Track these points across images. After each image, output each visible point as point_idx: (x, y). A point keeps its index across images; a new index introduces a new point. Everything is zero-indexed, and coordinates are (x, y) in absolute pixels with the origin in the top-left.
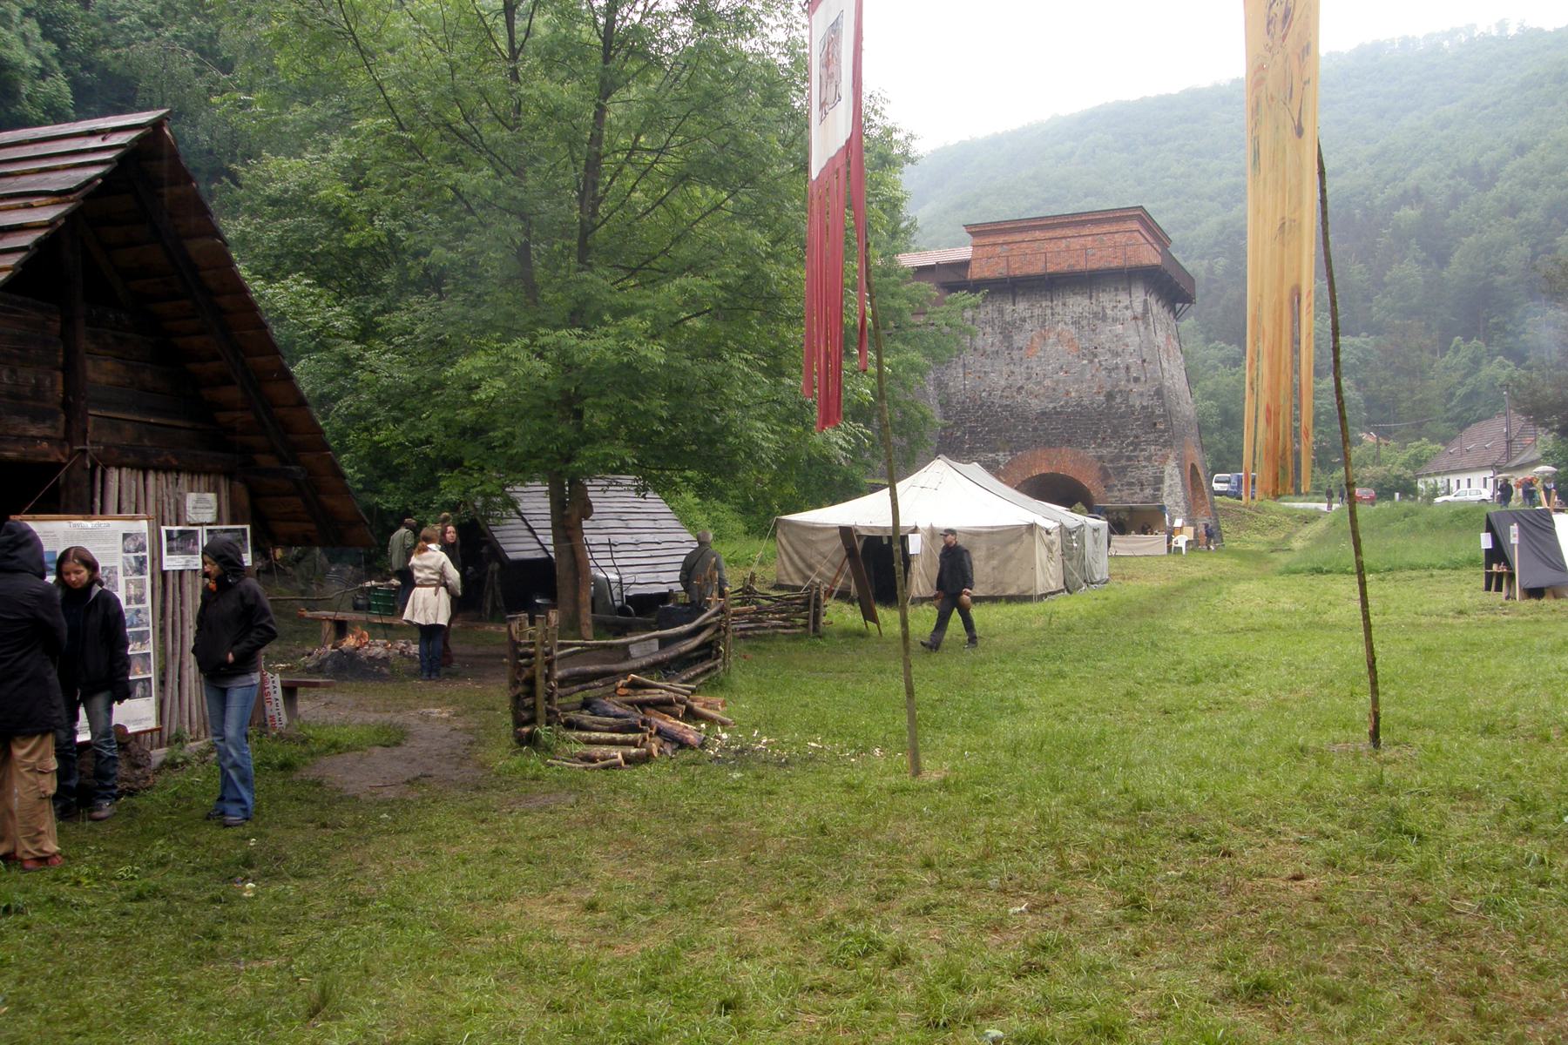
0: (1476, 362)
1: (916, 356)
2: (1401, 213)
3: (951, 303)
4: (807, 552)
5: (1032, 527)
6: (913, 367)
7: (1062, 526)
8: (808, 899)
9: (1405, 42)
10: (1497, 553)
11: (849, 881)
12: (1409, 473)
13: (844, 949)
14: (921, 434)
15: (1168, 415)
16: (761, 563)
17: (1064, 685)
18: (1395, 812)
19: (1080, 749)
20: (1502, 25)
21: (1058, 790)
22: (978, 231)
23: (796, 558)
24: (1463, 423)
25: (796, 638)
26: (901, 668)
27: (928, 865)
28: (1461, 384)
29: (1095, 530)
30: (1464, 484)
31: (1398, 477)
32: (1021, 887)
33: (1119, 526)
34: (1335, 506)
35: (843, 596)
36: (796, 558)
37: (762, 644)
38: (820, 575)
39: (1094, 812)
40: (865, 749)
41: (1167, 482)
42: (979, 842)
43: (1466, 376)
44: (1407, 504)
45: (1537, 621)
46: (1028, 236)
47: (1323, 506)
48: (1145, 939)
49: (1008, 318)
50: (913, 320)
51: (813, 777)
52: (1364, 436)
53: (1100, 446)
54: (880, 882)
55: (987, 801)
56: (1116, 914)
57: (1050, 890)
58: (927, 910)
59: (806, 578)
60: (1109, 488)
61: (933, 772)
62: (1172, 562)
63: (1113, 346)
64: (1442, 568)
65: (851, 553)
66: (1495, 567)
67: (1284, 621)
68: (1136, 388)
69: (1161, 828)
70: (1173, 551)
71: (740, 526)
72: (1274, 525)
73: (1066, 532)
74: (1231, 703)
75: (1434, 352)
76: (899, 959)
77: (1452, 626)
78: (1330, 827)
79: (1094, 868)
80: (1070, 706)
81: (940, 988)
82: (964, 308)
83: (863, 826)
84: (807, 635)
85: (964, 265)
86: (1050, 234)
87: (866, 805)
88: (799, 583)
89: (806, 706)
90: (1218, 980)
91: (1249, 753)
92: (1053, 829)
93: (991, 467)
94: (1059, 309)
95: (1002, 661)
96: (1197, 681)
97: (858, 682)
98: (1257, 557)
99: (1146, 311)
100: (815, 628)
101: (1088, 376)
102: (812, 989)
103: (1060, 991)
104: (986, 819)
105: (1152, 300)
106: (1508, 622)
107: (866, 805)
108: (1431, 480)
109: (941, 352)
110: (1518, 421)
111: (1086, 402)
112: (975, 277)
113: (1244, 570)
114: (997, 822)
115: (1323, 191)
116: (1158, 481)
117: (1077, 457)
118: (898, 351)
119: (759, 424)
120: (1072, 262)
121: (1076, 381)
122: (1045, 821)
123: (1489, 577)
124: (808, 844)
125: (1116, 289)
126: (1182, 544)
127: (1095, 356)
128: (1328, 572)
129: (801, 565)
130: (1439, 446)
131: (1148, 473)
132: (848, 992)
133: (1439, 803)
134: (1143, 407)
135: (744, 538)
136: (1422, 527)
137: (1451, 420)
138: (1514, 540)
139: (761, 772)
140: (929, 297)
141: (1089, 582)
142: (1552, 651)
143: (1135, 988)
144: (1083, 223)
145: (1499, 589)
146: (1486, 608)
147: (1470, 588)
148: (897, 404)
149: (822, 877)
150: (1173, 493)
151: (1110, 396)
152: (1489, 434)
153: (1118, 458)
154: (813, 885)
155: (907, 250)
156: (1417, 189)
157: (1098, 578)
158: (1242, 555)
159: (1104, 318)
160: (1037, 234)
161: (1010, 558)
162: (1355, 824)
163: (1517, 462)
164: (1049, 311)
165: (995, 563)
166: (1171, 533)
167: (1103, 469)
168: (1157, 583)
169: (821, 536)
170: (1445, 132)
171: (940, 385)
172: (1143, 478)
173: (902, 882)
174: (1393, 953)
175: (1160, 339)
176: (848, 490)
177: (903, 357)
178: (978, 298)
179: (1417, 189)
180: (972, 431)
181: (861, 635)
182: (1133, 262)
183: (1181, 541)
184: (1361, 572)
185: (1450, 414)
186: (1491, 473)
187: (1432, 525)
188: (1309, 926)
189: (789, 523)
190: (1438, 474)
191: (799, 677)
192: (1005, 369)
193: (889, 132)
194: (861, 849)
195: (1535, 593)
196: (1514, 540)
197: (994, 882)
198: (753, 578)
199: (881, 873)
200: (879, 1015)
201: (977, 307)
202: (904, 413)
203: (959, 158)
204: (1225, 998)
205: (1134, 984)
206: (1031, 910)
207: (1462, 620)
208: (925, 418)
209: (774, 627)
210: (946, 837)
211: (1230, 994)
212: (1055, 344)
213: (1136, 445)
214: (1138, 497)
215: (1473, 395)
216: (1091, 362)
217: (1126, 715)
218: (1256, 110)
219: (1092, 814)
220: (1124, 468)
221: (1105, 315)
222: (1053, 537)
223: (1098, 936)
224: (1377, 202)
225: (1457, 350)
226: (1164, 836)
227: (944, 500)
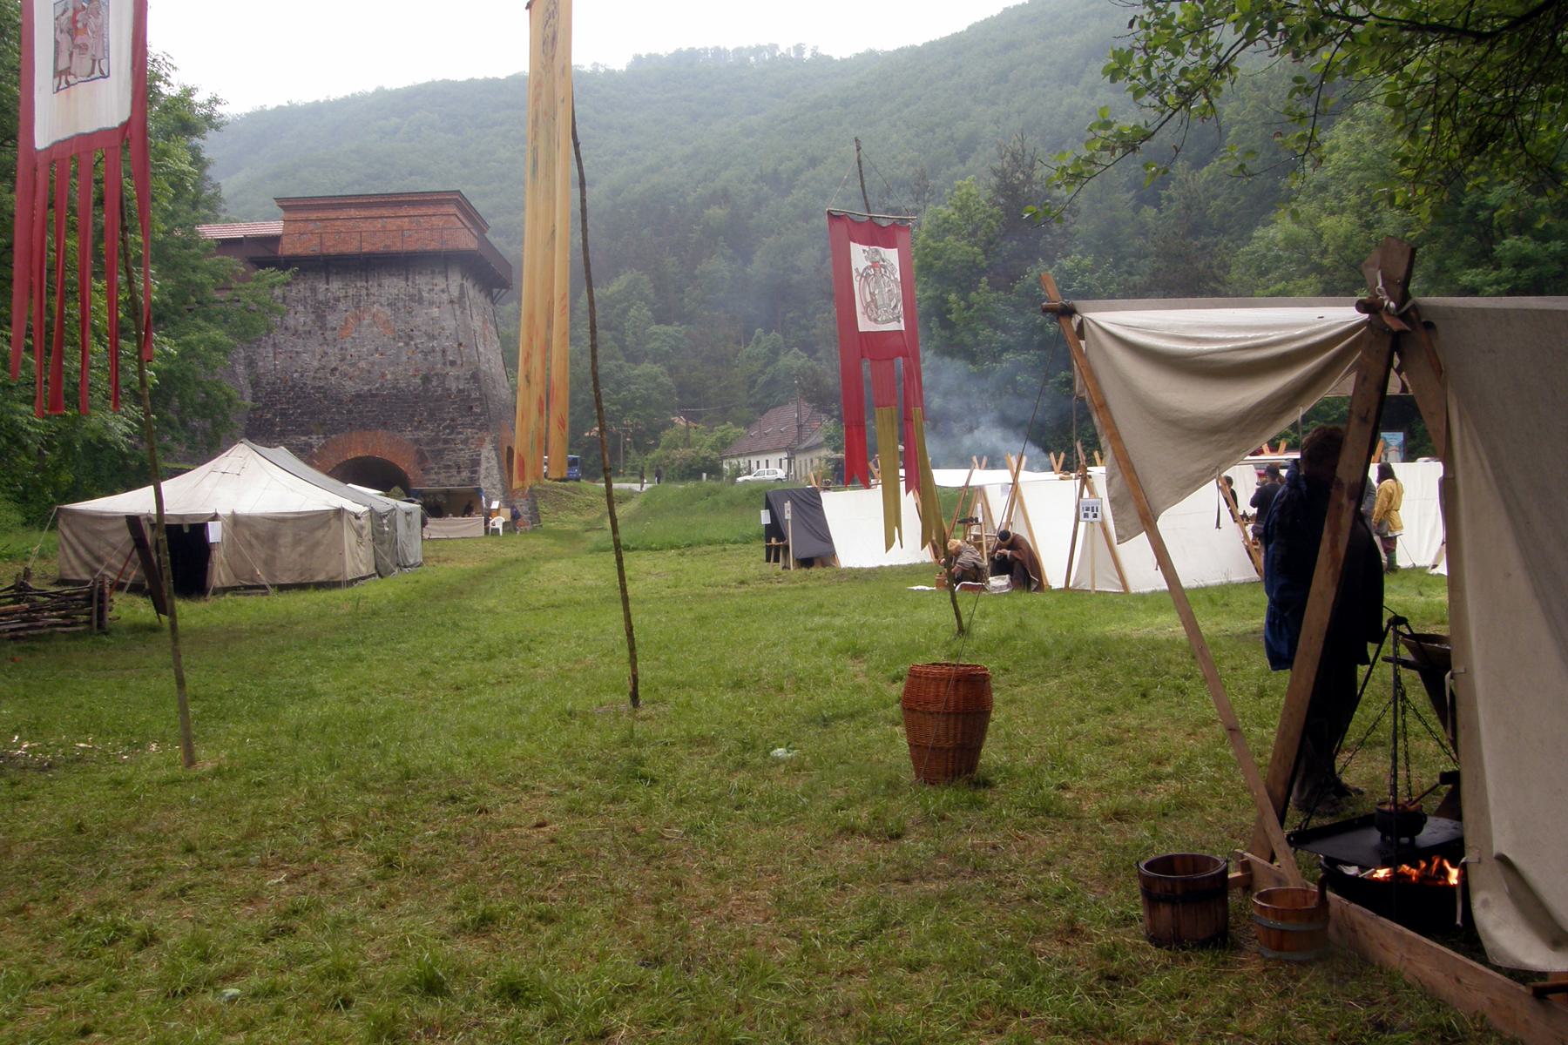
0: (775, 352)
1: (218, 334)
3: (258, 280)
4: (95, 545)
5: (340, 512)
6: (216, 346)
7: (372, 510)
8: (56, 898)
9: (718, 52)
10: (775, 529)
11: (104, 875)
12: (715, 455)
13: (88, 939)
14: (226, 416)
15: (484, 399)
16: (42, 556)
17: (360, 668)
18: (638, 761)
19: (364, 726)
20: (799, 49)
21: (332, 768)
22: (290, 206)
23: (82, 550)
24: (762, 408)
25: (75, 636)
26: (170, 659)
27: (190, 850)
28: (762, 372)
29: (408, 514)
30: (763, 464)
31: (705, 459)
32: (283, 860)
33: (435, 508)
34: (646, 486)
35: (136, 589)
36: (82, 550)
37: (37, 645)
38: (110, 567)
39: (364, 785)
40: (140, 745)
41: (484, 465)
42: (245, 823)
43: (766, 365)
44: (713, 484)
45: (804, 588)
46: (343, 214)
47: (636, 487)
48: (391, 893)
49: (321, 297)
50: (217, 296)
51: (78, 778)
52: (676, 419)
53: (416, 429)
54: (137, 872)
55: (259, 784)
56: (368, 875)
57: (310, 860)
58: (183, 892)
59: (94, 571)
60: (426, 471)
61: (207, 760)
62: (489, 544)
63: (430, 330)
64: (735, 542)
65: (139, 542)
66: (773, 540)
67: (581, 596)
68: (453, 372)
69: (425, 794)
70: (490, 532)
71: (18, 517)
72: (590, 506)
73: (375, 515)
74: (519, 675)
75: (739, 343)
76: (147, 941)
77: (733, 595)
78: (576, 779)
79: (356, 836)
80: (365, 688)
81: (184, 961)
82: (273, 286)
83: (124, 820)
84: (89, 632)
85: (275, 240)
86: (364, 213)
87: (132, 798)
88: (86, 577)
89: (80, 706)
90: (451, 919)
91: (524, 720)
92: (322, 804)
93: (304, 454)
94: (374, 290)
95: (302, 649)
96: (491, 657)
97: (144, 678)
98: (572, 537)
99: (462, 294)
100: (100, 625)
101: (404, 358)
102: (48, 983)
103: (303, 947)
104: (255, 801)
105: (468, 284)
107: (132, 798)
108: (734, 461)
109: (248, 331)
110: (807, 409)
111: (402, 384)
112: (287, 253)
113: (557, 549)
114: (266, 802)
115: (583, 201)
116: (475, 463)
117: (396, 439)
118: (200, 329)
119: (24, 408)
120: (388, 242)
121: (391, 364)
122: (313, 797)
123: (769, 549)
124: (61, 845)
125: (433, 272)
126: (499, 526)
127: (411, 338)
128: (634, 549)
129: (87, 557)
131: (465, 455)
132: (88, 979)
133: (679, 751)
134: (460, 391)
135: (21, 530)
136: (722, 504)
138: (788, 516)
139: (17, 778)
140: (235, 272)
141: (402, 566)
143: (375, 934)
144: (399, 204)
145: (777, 560)
146: (766, 578)
147: (753, 560)
148: (199, 384)
149: (73, 875)
150: (489, 477)
151: (426, 379)
152: (787, 416)
153: (434, 441)
154: (64, 884)
155: (216, 220)
157: (412, 561)
158: (558, 535)
159: (420, 301)
160: (352, 212)
161: (317, 544)
162: (601, 776)
163: (807, 444)
164: (364, 292)
165: (302, 549)
166: (489, 514)
167: (420, 453)
168: (470, 565)
169: (111, 526)
171: (251, 364)
172: (460, 461)
173: (160, 868)
174: (607, 879)
175: (477, 323)
176: (147, 474)
177: (204, 335)
178: (286, 276)
180: (283, 414)
181: (153, 629)
182: (450, 246)
183: (498, 522)
184: (619, 548)
185: (752, 400)
186: (785, 455)
187: (731, 503)
188: (541, 864)
189: (74, 512)
190: (740, 455)
191: (76, 676)
192: (319, 350)
193: (189, 92)
194: (123, 844)
195: (806, 563)
196: (788, 516)
197: (255, 859)
198: (27, 574)
199: (141, 863)
200: (116, 996)
201: (288, 284)
202: (207, 394)
203: (273, 126)
204: (455, 933)
205: (374, 932)
206: (288, 881)
207: (744, 589)
208: (230, 400)
209: (51, 625)
210: (211, 821)
211: (460, 930)
212: (370, 326)
213: (452, 429)
214: (456, 480)
215: (772, 382)
216: (407, 344)
217: (419, 694)
218: (535, 122)
219: (363, 787)
220: (440, 453)
221: (421, 298)
222: (363, 521)
223: (350, 895)
224: (690, 200)
225: (758, 341)
226: (427, 801)
227: (244, 486)
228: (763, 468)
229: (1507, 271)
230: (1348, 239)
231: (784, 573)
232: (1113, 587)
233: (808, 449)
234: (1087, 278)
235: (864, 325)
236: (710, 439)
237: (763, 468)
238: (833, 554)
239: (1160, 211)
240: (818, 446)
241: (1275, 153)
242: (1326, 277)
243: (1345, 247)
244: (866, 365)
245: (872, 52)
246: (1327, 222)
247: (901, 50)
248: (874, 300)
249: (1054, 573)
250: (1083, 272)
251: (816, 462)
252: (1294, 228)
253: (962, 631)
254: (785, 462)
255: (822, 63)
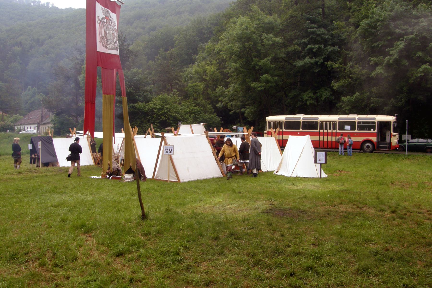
2: (15, 48)
10: (34, 151)
12: (12, 124)
20: (48, 3)
24: (30, 111)
30: (29, 128)
31: (9, 125)
43: (31, 98)
45: (46, 176)
66: (33, 156)
75: (22, 90)
77: (14, 180)
106: (36, 177)
108: (19, 127)
110: (45, 111)
123: (31, 159)
130: (22, 117)
137: (26, 110)
138: (40, 147)
142: (50, 192)
145: (34, 163)
146: (30, 171)
152: (37, 114)
156: (21, 42)
170: (30, 28)
179: (21, 42)
190: (21, 125)
195: (46, 164)
196: (40, 147)
207: (21, 176)
225: (29, 90)
228: (29, 129)
229: (263, 84)
230: (213, 72)
231: (37, 168)
232: (174, 180)
233: (45, 124)
234: (140, 76)
235: (100, 48)
236: (11, 119)
237: (29, 129)
238: (57, 161)
239: (155, 62)
240: (48, 123)
241: (188, 49)
242: (206, 83)
243: (212, 75)
244: (99, 68)
245: (71, 9)
246: (207, 67)
247: (80, 9)
248: (106, 36)
249: (149, 174)
250: (139, 73)
251: (47, 128)
252: (198, 69)
253: (144, 216)
254: (36, 128)
255: (55, 9)
